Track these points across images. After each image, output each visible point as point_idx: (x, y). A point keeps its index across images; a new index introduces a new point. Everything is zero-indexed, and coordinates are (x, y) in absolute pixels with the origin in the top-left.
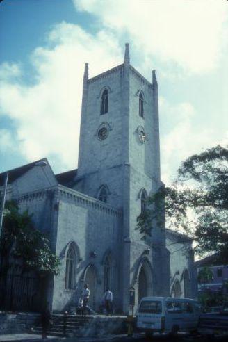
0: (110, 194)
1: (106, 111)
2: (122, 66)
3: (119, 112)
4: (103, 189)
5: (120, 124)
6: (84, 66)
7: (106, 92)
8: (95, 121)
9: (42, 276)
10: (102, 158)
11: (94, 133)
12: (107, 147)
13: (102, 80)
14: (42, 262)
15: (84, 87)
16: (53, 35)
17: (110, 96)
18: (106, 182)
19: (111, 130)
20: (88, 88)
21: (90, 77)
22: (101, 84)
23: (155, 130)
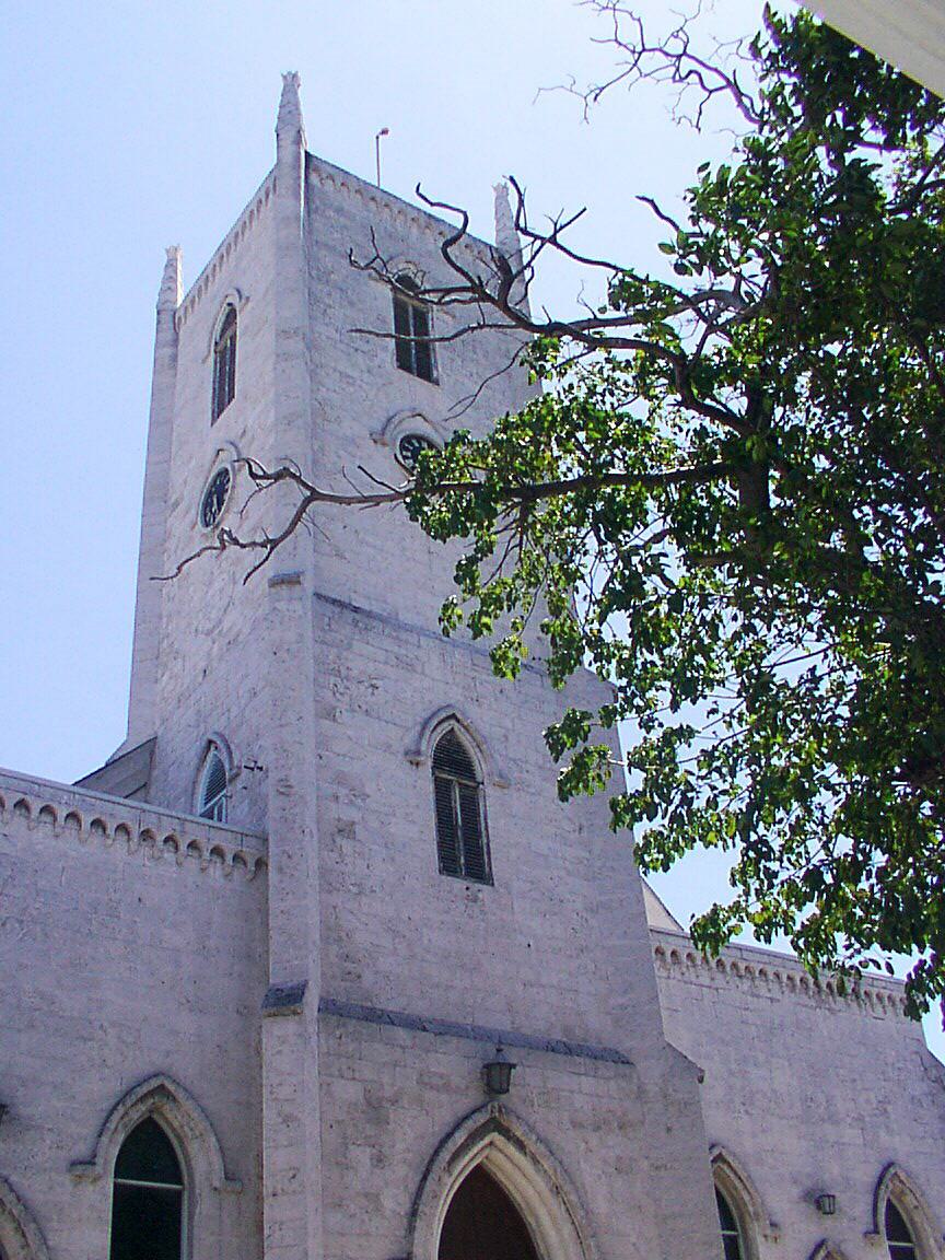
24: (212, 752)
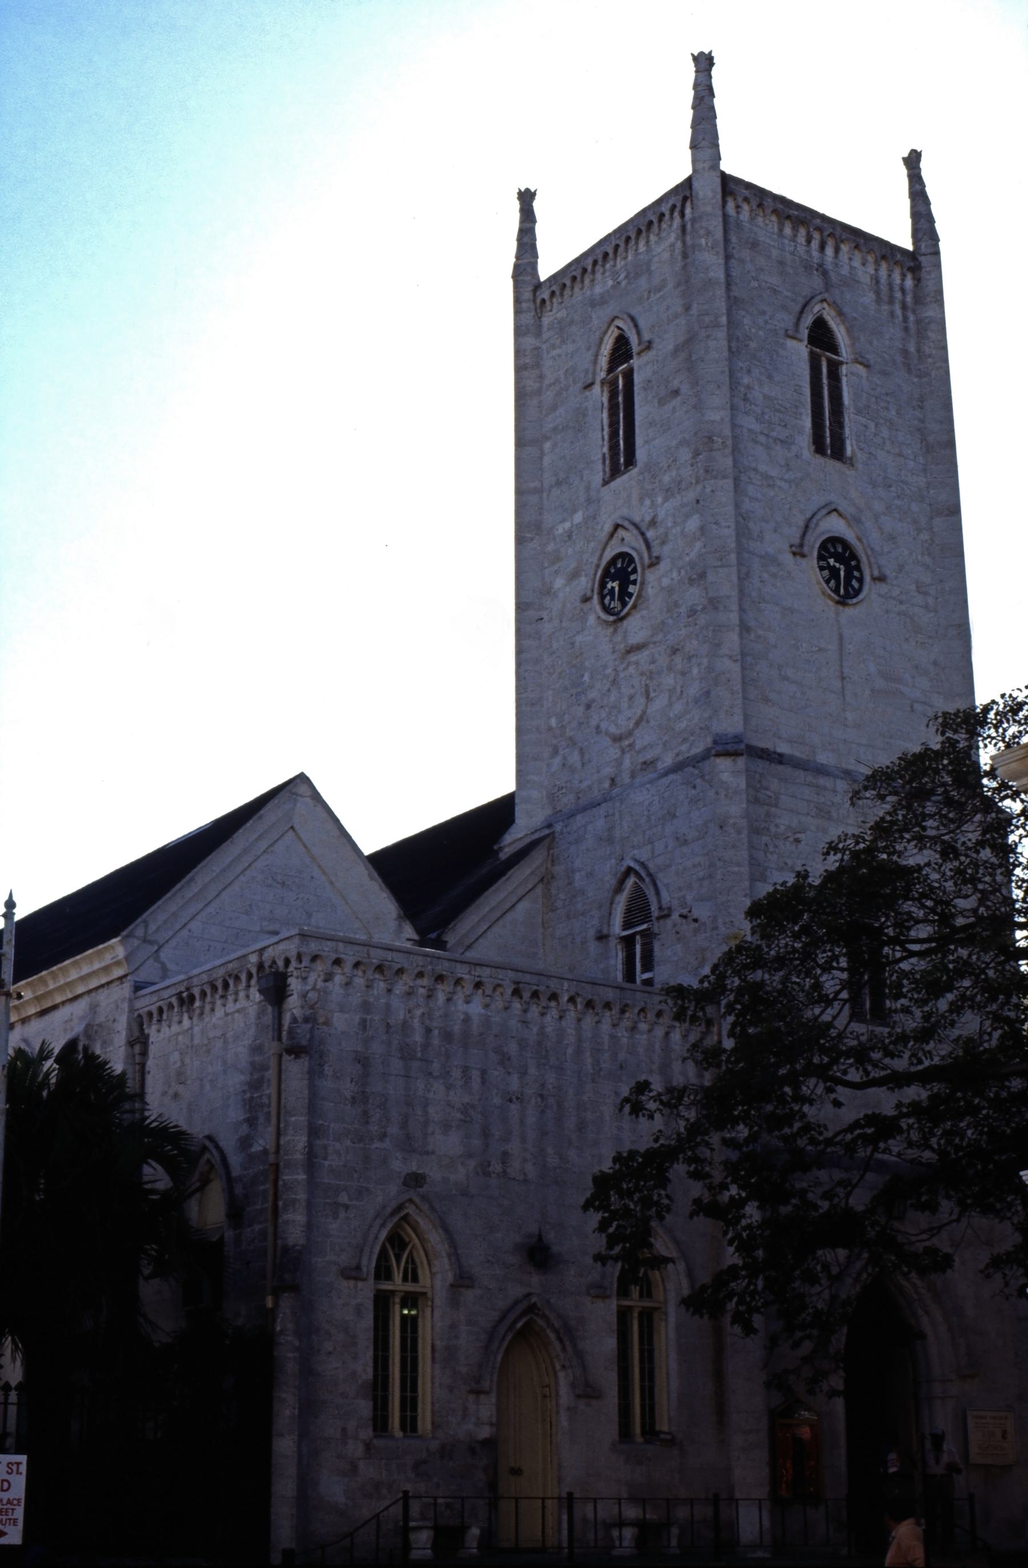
0: (665, 914)
1: (631, 460)
2: (684, 191)
3: (685, 455)
4: (637, 889)
5: (693, 524)
6: (515, 207)
7: (622, 351)
8: (578, 517)
9: (662, 1266)
10: (623, 723)
11: (585, 583)
12: (643, 656)
13: (602, 284)
14: (938, 881)
15: (519, 332)
16: (288, 983)
17: (642, 367)
18: (644, 855)
19: (655, 562)
20: (539, 330)
21: (547, 267)
22: (593, 304)
23: (928, 449)
24: (631, 880)
